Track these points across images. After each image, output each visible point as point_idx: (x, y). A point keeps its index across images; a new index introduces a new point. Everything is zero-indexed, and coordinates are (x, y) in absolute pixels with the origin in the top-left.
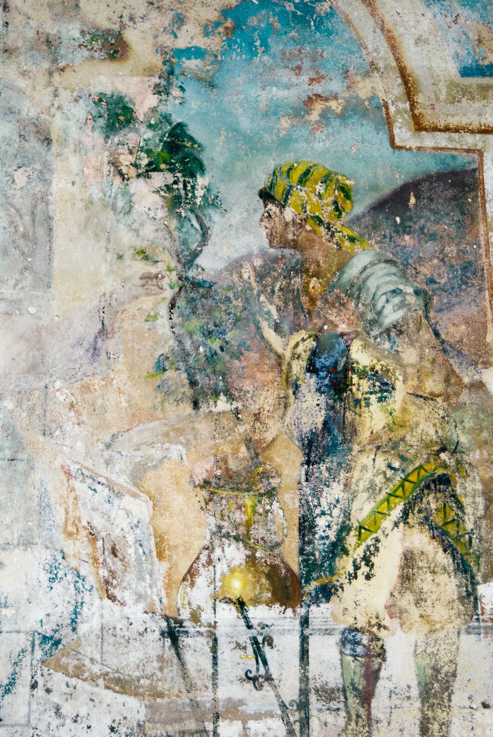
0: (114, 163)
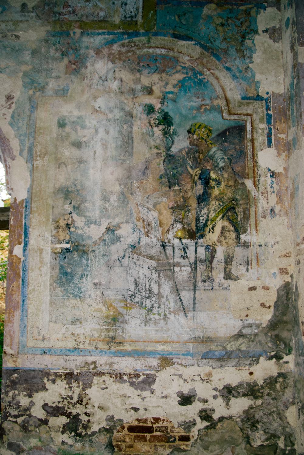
0: (149, 123)
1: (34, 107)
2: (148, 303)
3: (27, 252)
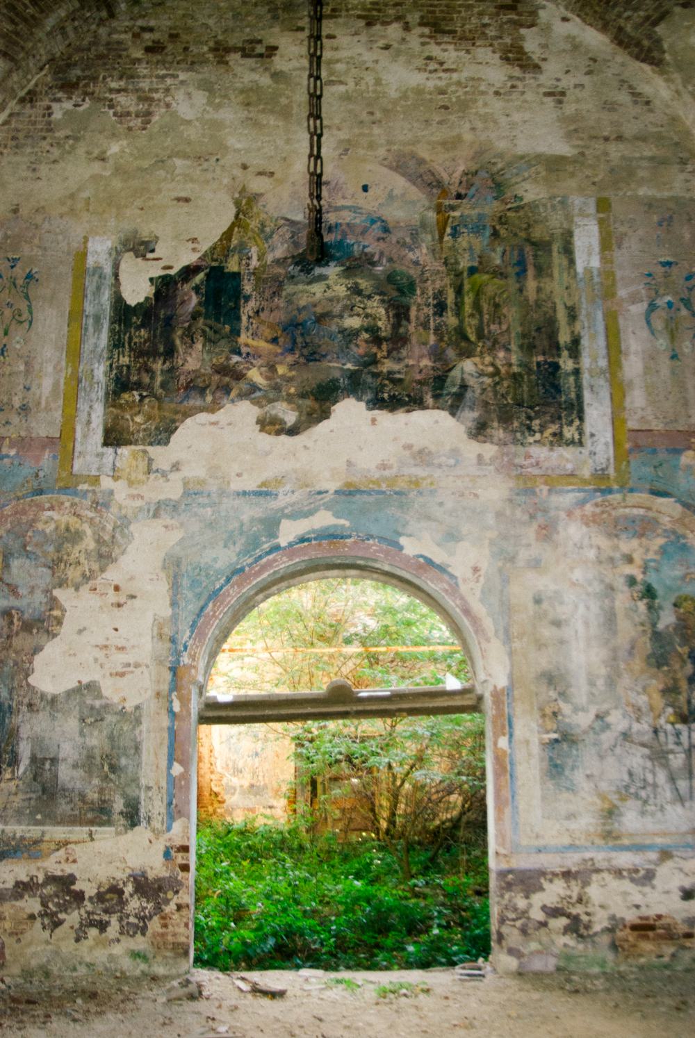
0: (632, 596)
1: (506, 581)
2: (643, 794)
3: (513, 744)
